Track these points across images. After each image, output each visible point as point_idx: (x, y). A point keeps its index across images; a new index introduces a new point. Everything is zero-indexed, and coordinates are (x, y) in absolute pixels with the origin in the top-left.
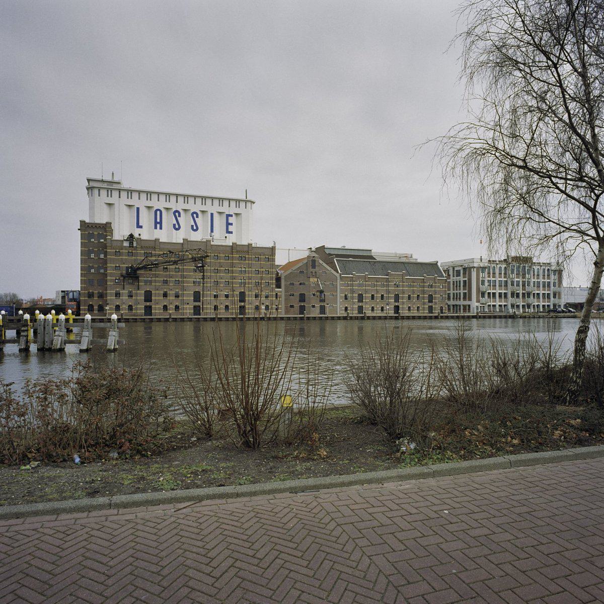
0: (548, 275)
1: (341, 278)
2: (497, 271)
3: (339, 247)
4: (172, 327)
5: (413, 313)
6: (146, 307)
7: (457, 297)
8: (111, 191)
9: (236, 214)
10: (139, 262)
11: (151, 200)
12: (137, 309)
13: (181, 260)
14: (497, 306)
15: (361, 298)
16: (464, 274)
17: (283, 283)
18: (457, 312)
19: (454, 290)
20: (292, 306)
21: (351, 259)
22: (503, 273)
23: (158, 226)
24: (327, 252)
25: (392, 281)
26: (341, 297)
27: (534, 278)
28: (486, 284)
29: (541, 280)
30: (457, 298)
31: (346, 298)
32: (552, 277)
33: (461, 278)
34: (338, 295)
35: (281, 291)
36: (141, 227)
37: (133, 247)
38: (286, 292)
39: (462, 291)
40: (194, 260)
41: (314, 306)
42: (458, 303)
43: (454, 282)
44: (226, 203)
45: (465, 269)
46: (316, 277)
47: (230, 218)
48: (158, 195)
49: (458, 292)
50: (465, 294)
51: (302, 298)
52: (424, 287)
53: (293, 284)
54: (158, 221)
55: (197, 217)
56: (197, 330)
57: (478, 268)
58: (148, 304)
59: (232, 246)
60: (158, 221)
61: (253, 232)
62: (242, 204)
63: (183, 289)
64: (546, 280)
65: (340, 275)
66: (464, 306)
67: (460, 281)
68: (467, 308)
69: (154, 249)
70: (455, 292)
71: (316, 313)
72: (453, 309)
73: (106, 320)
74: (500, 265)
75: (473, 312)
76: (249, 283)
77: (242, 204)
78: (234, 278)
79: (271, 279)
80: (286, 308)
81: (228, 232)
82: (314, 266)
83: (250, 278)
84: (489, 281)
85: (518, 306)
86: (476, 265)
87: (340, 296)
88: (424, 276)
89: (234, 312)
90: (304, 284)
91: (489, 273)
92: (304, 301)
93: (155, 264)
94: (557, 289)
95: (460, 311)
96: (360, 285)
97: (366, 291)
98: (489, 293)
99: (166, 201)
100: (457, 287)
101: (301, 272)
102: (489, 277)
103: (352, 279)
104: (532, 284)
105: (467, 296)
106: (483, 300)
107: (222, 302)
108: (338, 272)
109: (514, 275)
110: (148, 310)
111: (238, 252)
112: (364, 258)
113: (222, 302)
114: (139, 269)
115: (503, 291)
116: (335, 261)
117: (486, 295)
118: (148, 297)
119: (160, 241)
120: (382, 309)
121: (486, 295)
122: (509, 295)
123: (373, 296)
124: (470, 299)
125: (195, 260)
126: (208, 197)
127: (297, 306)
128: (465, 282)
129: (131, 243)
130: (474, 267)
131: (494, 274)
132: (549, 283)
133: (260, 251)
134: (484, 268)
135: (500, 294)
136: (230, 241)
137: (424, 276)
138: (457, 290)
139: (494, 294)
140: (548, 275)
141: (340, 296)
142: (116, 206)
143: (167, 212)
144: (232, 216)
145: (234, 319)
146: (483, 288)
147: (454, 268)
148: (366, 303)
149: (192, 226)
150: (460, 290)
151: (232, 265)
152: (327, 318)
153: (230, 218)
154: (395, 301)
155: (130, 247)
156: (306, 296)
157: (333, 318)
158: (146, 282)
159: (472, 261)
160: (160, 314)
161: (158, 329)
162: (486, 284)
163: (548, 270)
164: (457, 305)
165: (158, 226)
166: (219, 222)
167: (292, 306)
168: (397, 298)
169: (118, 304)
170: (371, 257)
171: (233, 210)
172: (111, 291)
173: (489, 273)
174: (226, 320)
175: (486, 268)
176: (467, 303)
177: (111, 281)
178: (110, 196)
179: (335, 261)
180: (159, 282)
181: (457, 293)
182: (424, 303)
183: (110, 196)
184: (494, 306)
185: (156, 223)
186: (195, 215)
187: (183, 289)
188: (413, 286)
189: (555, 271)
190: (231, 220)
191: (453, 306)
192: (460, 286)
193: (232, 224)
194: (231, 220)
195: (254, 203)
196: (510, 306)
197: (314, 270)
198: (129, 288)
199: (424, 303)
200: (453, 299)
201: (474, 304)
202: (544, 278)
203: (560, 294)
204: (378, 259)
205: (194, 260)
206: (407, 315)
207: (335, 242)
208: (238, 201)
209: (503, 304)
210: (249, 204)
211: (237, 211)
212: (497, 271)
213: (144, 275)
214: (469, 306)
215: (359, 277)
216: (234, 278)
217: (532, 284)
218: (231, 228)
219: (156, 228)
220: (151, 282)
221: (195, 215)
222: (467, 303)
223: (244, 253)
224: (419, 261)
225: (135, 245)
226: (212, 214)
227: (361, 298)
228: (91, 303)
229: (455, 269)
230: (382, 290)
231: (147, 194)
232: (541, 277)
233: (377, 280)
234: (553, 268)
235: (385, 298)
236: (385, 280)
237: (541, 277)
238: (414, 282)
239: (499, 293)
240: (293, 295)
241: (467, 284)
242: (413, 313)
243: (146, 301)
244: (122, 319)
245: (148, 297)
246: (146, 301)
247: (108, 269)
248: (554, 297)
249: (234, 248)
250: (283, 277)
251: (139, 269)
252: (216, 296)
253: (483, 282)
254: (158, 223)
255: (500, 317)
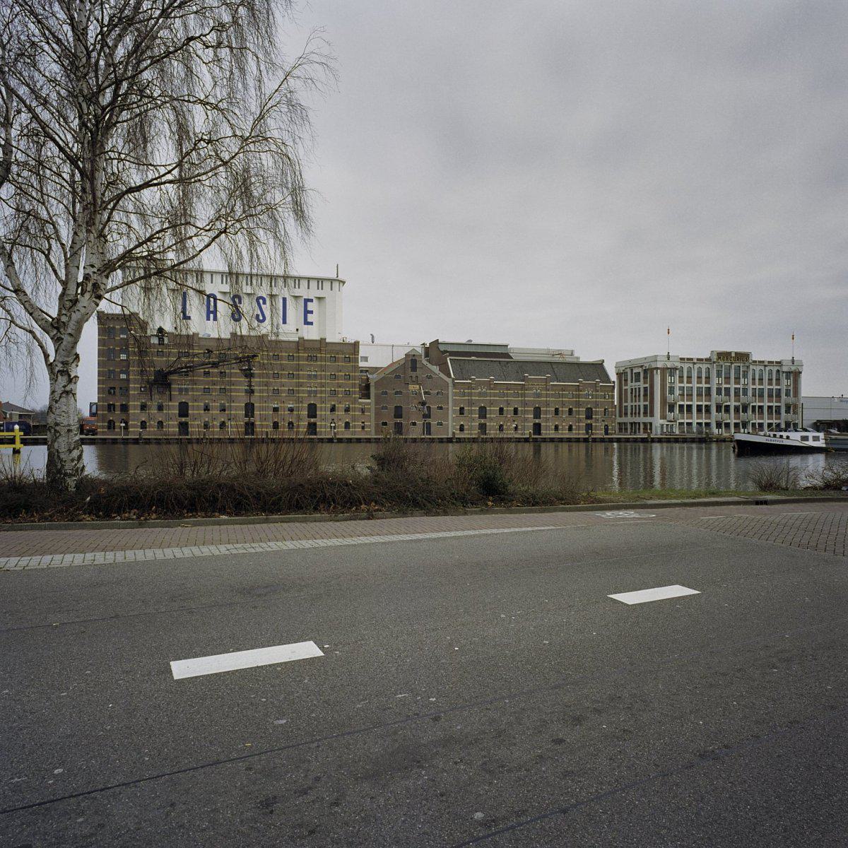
0: (778, 380)
1: (454, 384)
2: (695, 375)
3: (464, 341)
4: (564, 447)
5: (562, 434)
6: (181, 424)
7: (635, 412)
8: (322, 282)
9: (319, 299)
10: (170, 363)
11: (322, 289)
12: (213, 427)
13: (222, 360)
14: (695, 425)
15: (483, 412)
16: (645, 378)
17: (373, 391)
18: (635, 432)
19: (632, 401)
20: (385, 424)
21: (473, 358)
22: (704, 376)
23: (212, 316)
24: (442, 348)
25: (531, 389)
26: (454, 411)
27: (754, 384)
28: (677, 392)
29: (766, 387)
30: (635, 413)
31: (462, 411)
32: (784, 382)
33: (641, 385)
34: (450, 409)
35: (370, 401)
36: (311, 323)
37: (163, 344)
38: (377, 403)
39: (642, 403)
40: (240, 360)
41: (414, 424)
42: (636, 420)
43: (632, 389)
44: (304, 283)
45: (645, 371)
46: (418, 384)
47: (309, 303)
48: (309, 281)
49: (637, 404)
50: (645, 407)
51: (398, 412)
52: (579, 396)
53: (386, 393)
54: (212, 309)
55: (264, 303)
56: (537, 451)
57: (664, 370)
58: (312, 420)
59: (298, 342)
60: (212, 309)
61: (341, 323)
62: (327, 285)
63: (231, 400)
64: (775, 387)
65: (453, 380)
66: (645, 424)
67: (639, 388)
68: (648, 427)
69: (320, 350)
70: (634, 404)
71: (416, 432)
72: (631, 429)
73: (673, 440)
74: (701, 365)
75: (656, 433)
76: (321, 392)
77: (327, 285)
78: (300, 385)
79: (354, 386)
80: (377, 425)
81: (307, 323)
82: (414, 368)
83: (322, 385)
84: (682, 389)
85: (727, 425)
86: (659, 365)
87: (452, 410)
88: (579, 382)
89: (528, 432)
90: (400, 393)
91: (681, 377)
92: (186, 415)
93: (190, 367)
94: (791, 400)
95: (639, 432)
96: (480, 394)
97: (491, 403)
98: (754, 407)
99: (318, 289)
100: (635, 396)
101: (398, 377)
102: (681, 382)
103: (469, 386)
104: (750, 393)
105: (649, 411)
106: (670, 416)
107: (285, 417)
108: (449, 375)
109: (722, 380)
110: (184, 427)
111: (305, 350)
112: (496, 357)
113: (216, 417)
114: (170, 373)
115: (704, 403)
116: (449, 361)
117: (677, 410)
118: (184, 410)
119: (328, 341)
120: (570, 428)
121: (677, 410)
122: (714, 409)
123: (501, 410)
124: (652, 415)
125: (241, 362)
126: (312, 278)
127: (391, 422)
128: (645, 389)
129: (161, 340)
130: (657, 368)
131: (689, 377)
132: (709, 389)
133: (338, 348)
134: (672, 371)
135: (699, 408)
136: (311, 334)
137: (579, 382)
138: (636, 401)
139: (689, 407)
140: (778, 380)
141: (452, 410)
142: (327, 300)
143: (319, 302)
144: (311, 301)
145: (526, 440)
146: (670, 398)
147: (632, 370)
148: (491, 419)
149: (258, 316)
150: (639, 401)
151: (298, 368)
152: (432, 440)
153: (309, 303)
154: (535, 417)
155: (159, 344)
156: (403, 410)
157: (441, 441)
158: (180, 390)
159: (655, 359)
160: (103, 433)
161: (548, 450)
162: (677, 392)
163: (778, 371)
164: (635, 423)
165: (212, 316)
166: (294, 313)
167: (385, 424)
168: (537, 412)
169: (143, 419)
170: (507, 355)
171: (313, 292)
172: (134, 405)
173: (681, 377)
174: (440, 442)
175: (676, 369)
176: (648, 419)
177: (135, 389)
178: (297, 286)
179: (449, 361)
180: (197, 390)
181: (632, 406)
182: (580, 420)
183: (297, 286)
184: (689, 424)
185: (209, 313)
186: (261, 301)
187: (231, 400)
188: (563, 396)
189: (788, 373)
190: (310, 306)
191: (631, 424)
192: (639, 395)
193: (311, 312)
194: (310, 306)
195: (344, 283)
196: (714, 425)
197: (414, 374)
198: (157, 399)
199: (580, 420)
200: (632, 414)
201: (658, 421)
202: (770, 384)
203: (796, 406)
204: (516, 358)
205: (240, 360)
206: (567, 436)
207: (453, 334)
208: (320, 281)
209: (704, 421)
210: (336, 285)
211: (320, 294)
212: (695, 375)
213: (177, 382)
214: (651, 424)
215: (480, 383)
216: (300, 385)
217: (750, 393)
218: (310, 318)
219: (208, 319)
220: (187, 390)
221: (261, 301)
222: (648, 419)
223: (316, 350)
224: (583, 359)
225: (166, 341)
226: (284, 300)
227: (483, 412)
228: (111, 418)
229: (634, 371)
230: (516, 401)
231: (318, 282)
232: (695, 379)
233: (508, 387)
234: (785, 369)
235: (519, 412)
236: (574, 389)
237: (695, 379)
238: (563, 390)
239: (698, 406)
240: (386, 408)
241: (649, 393)
242: (562, 434)
243: (181, 415)
244: (141, 439)
245: (184, 410)
246: (181, 415)
247: (131, 373)
248: (787, 411)
249: (301, 344)
250: (372, 384)
251: (170, 373)
252: (276, 410)
253: (672, 391)
254: (212, 312)
255: (685, 441)
